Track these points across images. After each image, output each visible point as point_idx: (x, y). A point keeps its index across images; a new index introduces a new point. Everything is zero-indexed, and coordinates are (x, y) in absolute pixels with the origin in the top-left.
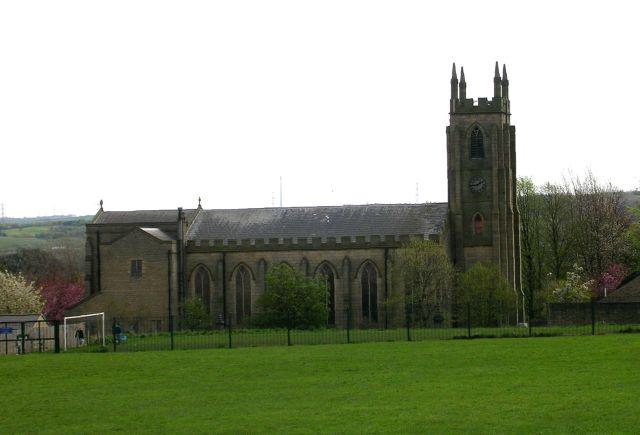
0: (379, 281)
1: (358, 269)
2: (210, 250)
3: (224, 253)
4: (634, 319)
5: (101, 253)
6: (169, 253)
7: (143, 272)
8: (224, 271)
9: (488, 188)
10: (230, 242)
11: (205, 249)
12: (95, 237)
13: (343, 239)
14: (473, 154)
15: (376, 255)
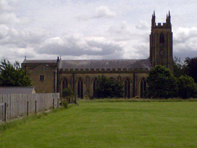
0: (131, 85)
2: (69, 73)
3: (74, 74)
4: (196, 97)
6: (55, 73)
7: (44, 79)
9: (166, 54)
10: (76, 69)
11: (66, 72)
13: (102, 69)
14: (160, 42)
15: (131, 76)
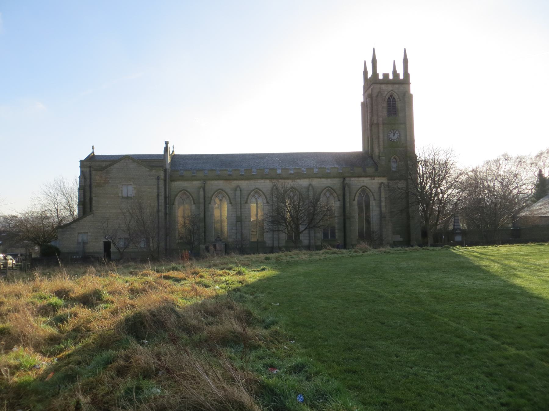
1: (356, 194)
5: (264, 192)
8: (204, 197)
12: (88, 170)
